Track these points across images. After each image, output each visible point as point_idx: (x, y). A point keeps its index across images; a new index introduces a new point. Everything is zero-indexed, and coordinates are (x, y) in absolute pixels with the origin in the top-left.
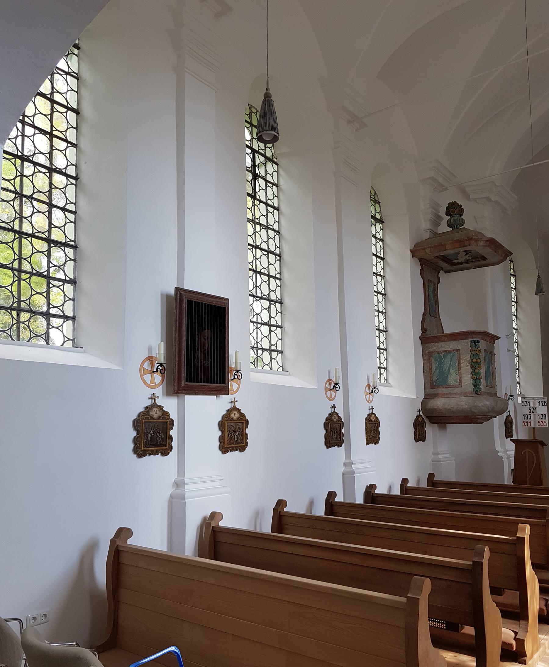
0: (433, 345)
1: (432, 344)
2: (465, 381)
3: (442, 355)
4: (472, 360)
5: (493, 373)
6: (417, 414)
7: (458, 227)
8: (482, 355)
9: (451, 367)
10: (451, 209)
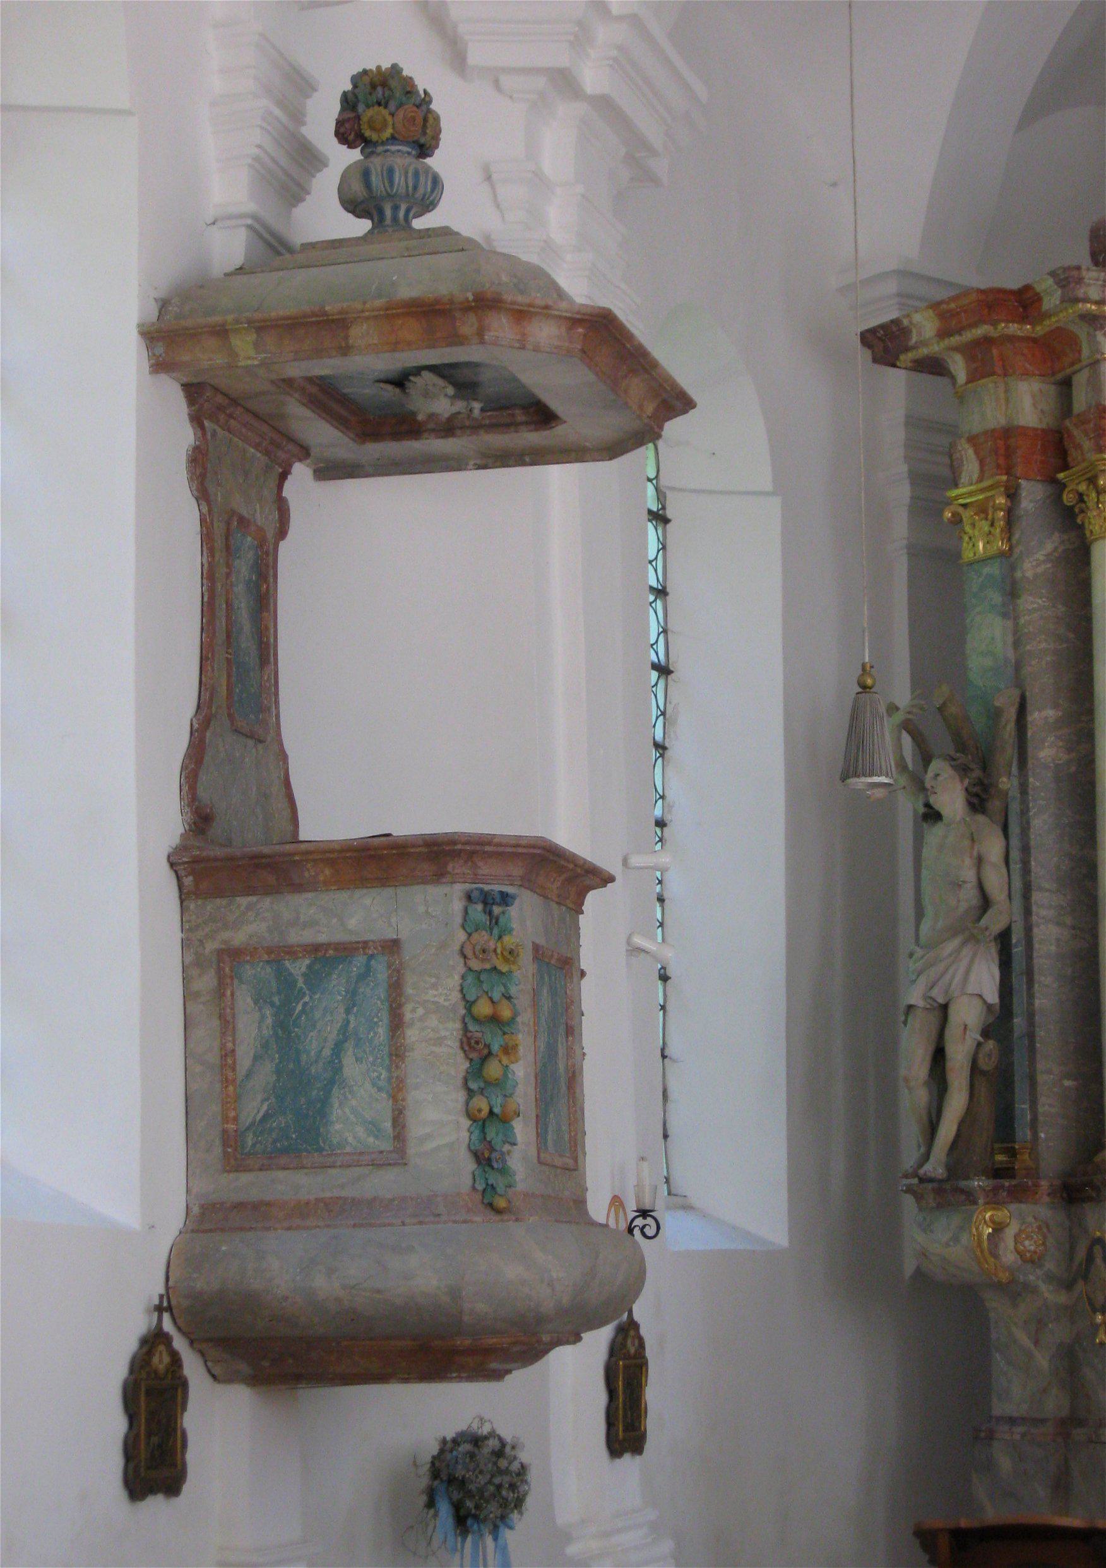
0: (249, 907)
1: (244, 901)
2: (428, 1130)
3: (298, 968)
4: (469, 1005)
5: (573, 1079)
6: (138, 1324)
7: (401, 214)
8: (525, 971)
9: (349, 1046)
10: (368, 106)
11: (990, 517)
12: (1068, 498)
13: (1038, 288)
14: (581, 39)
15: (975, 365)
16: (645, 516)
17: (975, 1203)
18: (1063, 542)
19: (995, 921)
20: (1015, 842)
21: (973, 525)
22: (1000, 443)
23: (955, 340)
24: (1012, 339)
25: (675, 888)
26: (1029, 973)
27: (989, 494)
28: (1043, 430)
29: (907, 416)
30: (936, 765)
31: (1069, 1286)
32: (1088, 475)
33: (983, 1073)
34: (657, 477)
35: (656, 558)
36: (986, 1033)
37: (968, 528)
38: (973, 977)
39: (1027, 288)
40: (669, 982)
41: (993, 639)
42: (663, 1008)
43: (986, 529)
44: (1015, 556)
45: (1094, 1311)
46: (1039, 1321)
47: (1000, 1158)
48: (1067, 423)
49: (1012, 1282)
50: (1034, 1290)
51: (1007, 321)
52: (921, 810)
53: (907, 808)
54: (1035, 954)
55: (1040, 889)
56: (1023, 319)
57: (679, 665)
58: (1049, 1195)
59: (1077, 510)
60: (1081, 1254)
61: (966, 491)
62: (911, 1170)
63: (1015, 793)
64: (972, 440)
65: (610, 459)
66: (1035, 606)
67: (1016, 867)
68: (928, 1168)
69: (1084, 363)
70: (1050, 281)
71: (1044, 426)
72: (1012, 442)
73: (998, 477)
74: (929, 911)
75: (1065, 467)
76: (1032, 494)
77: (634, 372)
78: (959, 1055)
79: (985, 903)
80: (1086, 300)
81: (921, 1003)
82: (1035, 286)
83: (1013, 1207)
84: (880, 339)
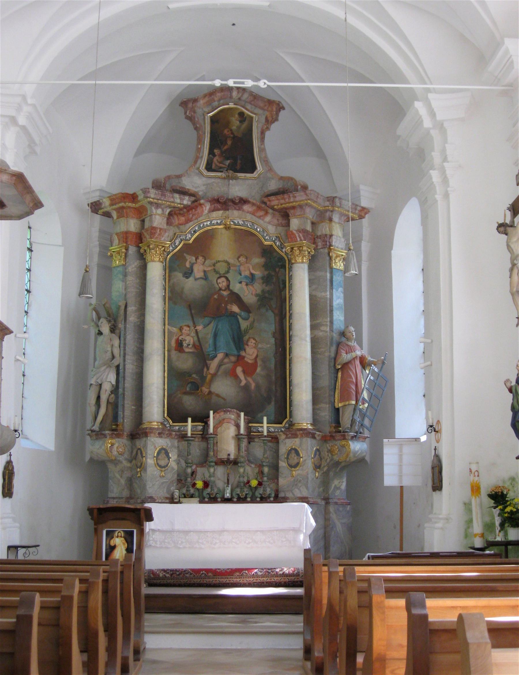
11: (120, 255)
12: (142, 251)
13: (137, 194)
14: (19, 109)
15: (119, 214)
16: (27, 249)
17: (106, 438)
18: (140, 263)
19: (116, 362)
20: (122, 342)
21: (116, 257)
22: (125, 235)
23: (114, 207)
24: (129, 207)
25: (28, 351)
26: (124, 377)
27: (121, 249)
28: (136, 233)
29: (99, 229)
30: (102, 320)
31: (131, 461)
32: (147, 245)
33: (110, 403)
34: (30, 239)
35: (28, 261)
36: (112, 392)
37: (114, 258)
38: (109, 377)
39: (134, 194)
40: (25, 377)
41: (119, 288)
42: (23, 383)
43: (119, 258)
44: (126, 266)
45: (137, 468)
46: (122, 471)
47: (114, 427)
48: (143, 231)
49: (115, 460)
50: (121, 462)
51: (129, 202)
52: (97, 332)
53: (93, 331)
54: (126, 372)
55: (128, 355)
56: (133, 202)
57: (30, 313)
58: (126, 437)
59: (144, 254)
60: (134, 452)
61: (115, 248)
62: (89, 429)
63: (123, 329)
64: (117, 234)
65: (19, 220)
66: (131, 279)
67: (122, 349)
68: (94, 428)
69: (148, 215)
70: (141, 192)
71: (137, 232)
72: (128, 235)
73: (123, 244)
74: (98, 358)
75: (142, 243)
76: (132, 250)
77: (28, 193)
78: (104, 397)
79: (113, 357)
80: (150, 198)
81: (94, 384)
82: (137, 193)
83: (117, 439)
84: (94, 206)
